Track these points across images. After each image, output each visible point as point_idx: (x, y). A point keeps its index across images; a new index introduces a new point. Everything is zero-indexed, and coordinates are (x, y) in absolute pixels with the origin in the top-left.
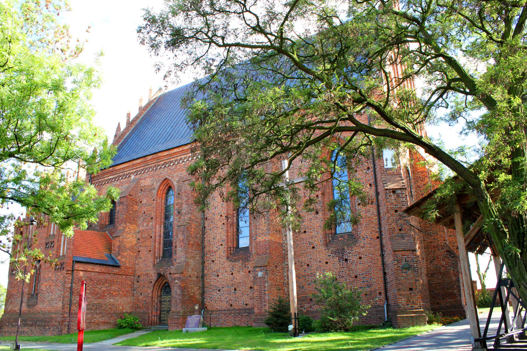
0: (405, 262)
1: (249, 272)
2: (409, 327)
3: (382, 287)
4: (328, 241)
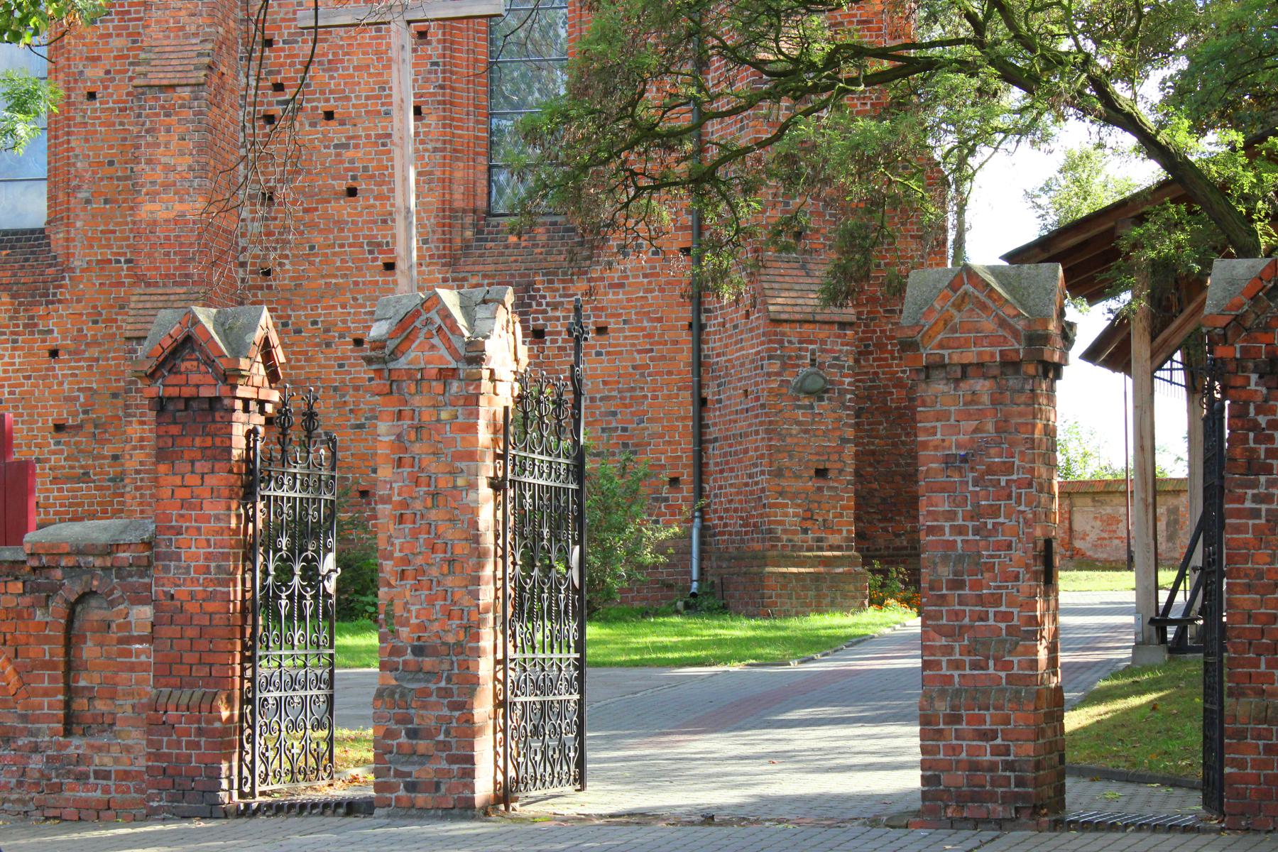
0: (809, 369)
1: (54, 353)
2: (806, 615)
3: (687, 459)
4: (458, 243)
